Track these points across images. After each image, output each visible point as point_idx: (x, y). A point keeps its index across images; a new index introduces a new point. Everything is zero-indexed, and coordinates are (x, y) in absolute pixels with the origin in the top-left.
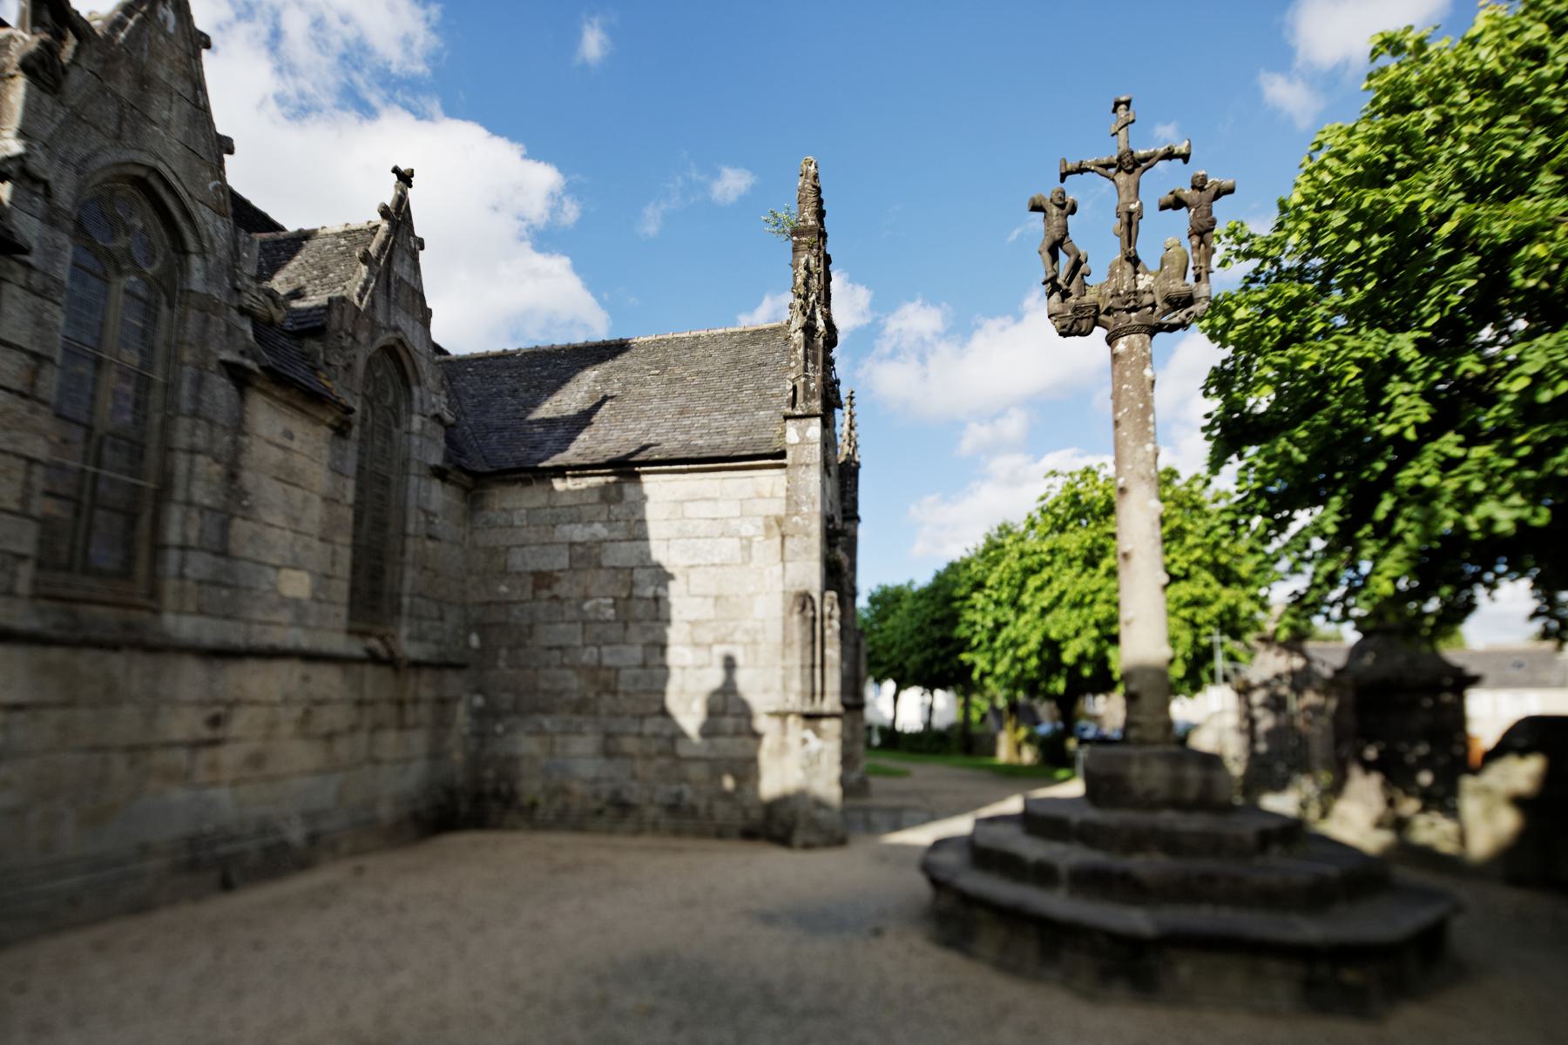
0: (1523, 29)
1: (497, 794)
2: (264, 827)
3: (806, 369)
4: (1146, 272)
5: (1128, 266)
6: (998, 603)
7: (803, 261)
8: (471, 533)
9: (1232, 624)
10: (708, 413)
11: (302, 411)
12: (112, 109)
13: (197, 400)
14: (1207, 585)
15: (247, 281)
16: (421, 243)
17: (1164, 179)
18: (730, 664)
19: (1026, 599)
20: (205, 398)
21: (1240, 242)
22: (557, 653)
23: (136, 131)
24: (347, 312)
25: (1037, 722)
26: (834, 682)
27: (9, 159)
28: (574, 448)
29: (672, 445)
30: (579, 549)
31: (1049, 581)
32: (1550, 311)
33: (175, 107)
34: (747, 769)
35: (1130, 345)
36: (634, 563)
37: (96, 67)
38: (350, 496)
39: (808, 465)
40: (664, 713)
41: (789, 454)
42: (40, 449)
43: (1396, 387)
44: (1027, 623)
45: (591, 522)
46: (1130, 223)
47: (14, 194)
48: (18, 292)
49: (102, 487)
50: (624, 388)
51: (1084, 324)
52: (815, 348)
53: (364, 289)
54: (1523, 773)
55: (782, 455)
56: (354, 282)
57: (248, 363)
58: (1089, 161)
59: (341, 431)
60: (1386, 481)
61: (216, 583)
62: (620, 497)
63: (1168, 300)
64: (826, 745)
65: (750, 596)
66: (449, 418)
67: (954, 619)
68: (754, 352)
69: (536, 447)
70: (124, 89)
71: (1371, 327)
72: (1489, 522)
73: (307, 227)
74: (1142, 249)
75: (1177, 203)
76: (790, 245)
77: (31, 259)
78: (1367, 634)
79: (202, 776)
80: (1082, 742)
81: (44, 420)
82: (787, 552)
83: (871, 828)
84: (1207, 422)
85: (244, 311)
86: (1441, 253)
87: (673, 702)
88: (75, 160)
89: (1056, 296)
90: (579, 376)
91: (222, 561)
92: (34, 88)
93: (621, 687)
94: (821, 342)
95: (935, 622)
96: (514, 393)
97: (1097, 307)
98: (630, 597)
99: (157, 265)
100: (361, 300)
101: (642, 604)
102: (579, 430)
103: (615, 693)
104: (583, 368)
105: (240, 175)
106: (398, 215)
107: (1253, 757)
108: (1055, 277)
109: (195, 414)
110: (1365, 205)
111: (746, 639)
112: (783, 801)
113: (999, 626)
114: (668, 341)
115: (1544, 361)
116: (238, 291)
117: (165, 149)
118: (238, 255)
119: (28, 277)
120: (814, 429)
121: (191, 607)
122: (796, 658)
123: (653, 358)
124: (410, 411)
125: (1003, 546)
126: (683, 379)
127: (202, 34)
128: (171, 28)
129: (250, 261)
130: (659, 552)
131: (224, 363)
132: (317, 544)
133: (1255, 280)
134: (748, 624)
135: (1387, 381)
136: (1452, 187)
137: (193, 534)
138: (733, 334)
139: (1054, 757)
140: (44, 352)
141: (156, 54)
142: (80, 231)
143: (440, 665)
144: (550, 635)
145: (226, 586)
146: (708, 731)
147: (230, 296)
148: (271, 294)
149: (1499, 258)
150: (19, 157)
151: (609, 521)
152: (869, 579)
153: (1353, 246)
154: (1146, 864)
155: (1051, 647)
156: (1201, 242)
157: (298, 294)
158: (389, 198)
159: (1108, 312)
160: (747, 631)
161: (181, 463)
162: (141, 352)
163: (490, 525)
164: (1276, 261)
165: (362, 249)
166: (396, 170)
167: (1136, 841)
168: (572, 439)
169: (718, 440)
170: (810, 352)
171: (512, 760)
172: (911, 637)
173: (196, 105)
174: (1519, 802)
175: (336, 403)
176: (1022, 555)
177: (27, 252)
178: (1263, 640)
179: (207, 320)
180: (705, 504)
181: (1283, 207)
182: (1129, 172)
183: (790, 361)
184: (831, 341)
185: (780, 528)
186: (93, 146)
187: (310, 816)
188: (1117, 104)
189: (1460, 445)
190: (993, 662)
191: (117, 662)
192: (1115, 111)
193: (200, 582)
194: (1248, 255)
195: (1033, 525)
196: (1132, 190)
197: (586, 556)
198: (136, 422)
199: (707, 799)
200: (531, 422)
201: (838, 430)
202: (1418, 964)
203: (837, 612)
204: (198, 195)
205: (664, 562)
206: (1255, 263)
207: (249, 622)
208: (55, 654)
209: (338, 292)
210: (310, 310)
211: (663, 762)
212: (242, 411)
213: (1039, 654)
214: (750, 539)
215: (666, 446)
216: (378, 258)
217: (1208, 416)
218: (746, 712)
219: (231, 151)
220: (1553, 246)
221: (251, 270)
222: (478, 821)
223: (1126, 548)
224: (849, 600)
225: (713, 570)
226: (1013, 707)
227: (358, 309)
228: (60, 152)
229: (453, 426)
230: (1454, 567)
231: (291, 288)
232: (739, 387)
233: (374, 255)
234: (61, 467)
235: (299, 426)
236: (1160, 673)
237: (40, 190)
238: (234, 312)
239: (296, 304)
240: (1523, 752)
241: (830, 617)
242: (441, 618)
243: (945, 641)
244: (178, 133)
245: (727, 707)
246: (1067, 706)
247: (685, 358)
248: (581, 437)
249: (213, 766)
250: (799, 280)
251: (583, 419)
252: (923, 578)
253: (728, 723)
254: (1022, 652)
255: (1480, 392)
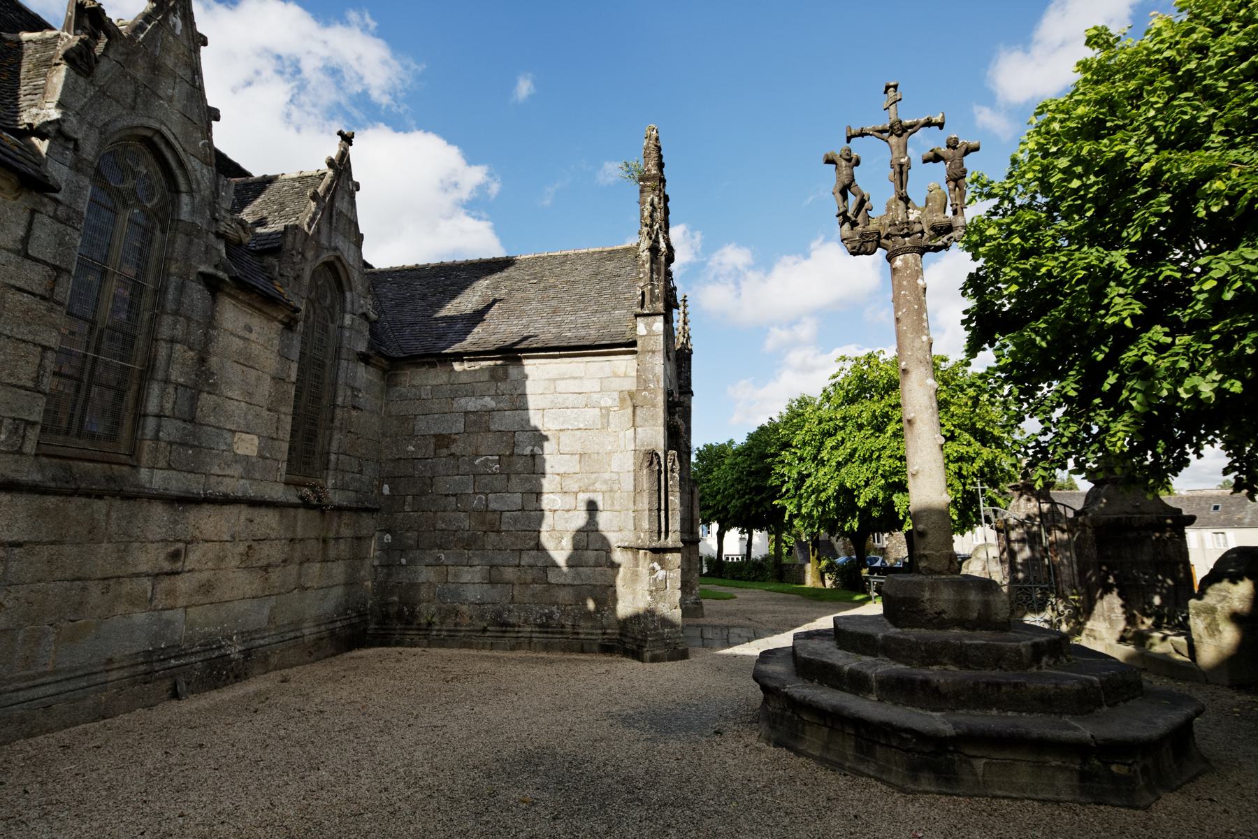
0: (1193, 30)
1: (400, 615)
2: (209, 643)
3: (651, 279)
4: (915, 208)
5: (901, 203)
6: (801, 459)
7: (649, 199)
8: (386, 405)
9: (991, 475)
10: (575, 312)
11: (260, 310)
12: (130, 88)
13: (179, 303)
14: (969, 444)
15: (223, 213)
16: (357, 186)
17: (924, 141)
18: (592, 507)
19: (824, 454)
20: (186, 301)
21: (984, 186)
22: (453, 499)
23: (146, 104)
24: (299, 237)
25: (837, 556)
26: (675, 524)
27: (50, 123)
28: (469, 339)
29: (547, 335)
30: (472, 417)
31: (843, 441)
32: (1229, 230)
33: (177, 87)
34: (607, 595)
35: (905, 262)
36: (516, 428)
37: (119, 58)
38: (294, 378)
39: (653, 352)
40: (539, 547)
41: (639, 343)
42: (52, 339)
43: (1114, 290)
44: (825, 474)
45: (482, 396)
46: (901, 172)
47: (50, 148)
48: (47, 220)
49: (100, 368)
50: (509, 293)
51: (869, 246)
52: (659, 264)
53: (312, 220)
54: (1239, 593)
55: (634, 344)
56: (305, 214)
57: (220, 274)
58: (868, 127)
59: (289, 326)
60: (1112, 361)
61: (183, 444)
62: (506, 374)
63: (933, 228)
64: (672, 572)
65: (609, 453)
66: (373, 316)
67: (768, 471)
68: (610, 266)
69: (440, 337)
70: (140, 75)
71: (1091, 246)
72: (1196, 391)
73: (270, 173)
74: (911, 191)
75: (936, 158)
76: (638, 188)
77: (59, 196)
78: (1098, 484)
79: (161, 601)
80: (873, 571)
81: (59, 317)
82: (638, 419)
83: (706, 644)
84: (966, 317)
85: (219, 235)
86: (1142, 191)
87: (546, 539)
88: (100, 124)
89: (847, 226)
90: (475, 284)
91: (189, 427)
92: (72, 73)
93: (504, 528)
94: (663, 259)
95: (750, 473)
96: (424, 297)
97: (879, 234)
98: (512, 454)
99: (155, 201)
100: (310, 227)
101: (522, 458)
102: (475, 325)
103: (499, 532)
104: (478, 278)
105: (224, 138)
106: (341, 166)
107: (1014, 581)
108: (846, 211)
109: (176, 313)
110: (1084, 152)
111: (605, 488)
112: (636, 617)
113: (802, 478)
114: (544, 258)
115: (1227, 269)
116: (216, 220)
117: (168, 119)
118: (218, 194)
119: (56, 210)
120: (658, 325)
121: (162, 463)
122: (644, 503)
123: (531, 271)
124: (343, 311)
125: (803, 414)
126: (555, 287)
127: (201, 35)
128: (178, 32)
129: (227, 197)
130: (535, 420)
131: (201, 274)
132: (265, 413)
133: (995, 214)
134: (607, 476)
135: (1107, 285)
136: (1148, 141)
137: (168, 406)
138: (594, 253)
139: (851, 584)
140: (63, 266)
141: (166, 50)
142: (98, 176)
143: (357, 510)
144: (445, 484)
145: (192, 447)
146: (573, 562)
147: (209, 224)
148: (242, 223)
149: (1188, 192)
150: (57, 121)
151: (497, 395)
152: (700, 438)
153: (1075, 184)
154: (940, 674)
155: (847, 495)
156: (956, 186)
157: (262, 222)
158: (334, 153)
159: (888, 237)
160: (606, 482)
161: (163, 350)
162: (138, 266)
163: (403, 398)
164: (1012, 201)
165: (312, 190)
166: (340, 133)
167: (932, 654)
168: (469, 332)
169: (583, 333)
170: (655, 266)
171: (414, 586)
172: (733, 485)
173: (193, 86)
174: (1236, 618)
175: (287, 305)
176: (820, 422)
177: (57, 191)
178: (1015, 488)
179: (190, 242)
180: (572, 382)
181: (1014, 161)
182: (899, 136)
183: (639, 273)
184: (670, 259)
185: (633, 401)
186: (114, 114)
187: (246, 635)
188: (888, 88)
189: (1166, 334)
190: (799, 507)
191: (99, 506)
192: (886, 92)
193: (171, 443)
194: (990, 196)
195: (828, 398)
196: (902, 149)
197: (478, 422)
198: (129, 318)
199: (574, 619)
200: (437, 319)
201: (675, 325)
202: (1170, 760)
203: (677, 466)
204: (191, 150)
205: (540, 427)
206: (996, 201)
207: (208, 475)
208: (51, 501)
209: (292, 221)
210: (270, 234)
211: (538, 587)
212: (213, 311)
213: (836, 499)
214: (608, 409)
215: (542, 337)
216: (324, 197)
217: (965, 312)
218: (606, 547)
219: (217, 119)
220: (1229, 183)
221: (227, 205)
222: (383, 640)
223: (910, 416)
224: (685, 457)
225: (578, 433)
226: (816, 543)
227: (307, 234)
228: (89, 118)
229: (376, 322)
230: (1171, 430)
231: (256, 218)
232: (599, 293)
233: (321, 194)
234: (69, 353)
235: (257, 322)
236: (943, 513)
237: (71, 146)
238: (212, 236)
239: (259, 230)
240: (1234, 580)
241: (672, 471)
242: (361, 472)
243: (760, 490)
244: (178, 105)
245: (589, 539)
246: (859, 541)
247: (557, 271)
248: (476, 330)
249: (171, 593)
250: (646, 214)
251: (478, 316)
252: (741, 440)
253: (590, 555)
254: (823, 496)
255: (1177, 293)
